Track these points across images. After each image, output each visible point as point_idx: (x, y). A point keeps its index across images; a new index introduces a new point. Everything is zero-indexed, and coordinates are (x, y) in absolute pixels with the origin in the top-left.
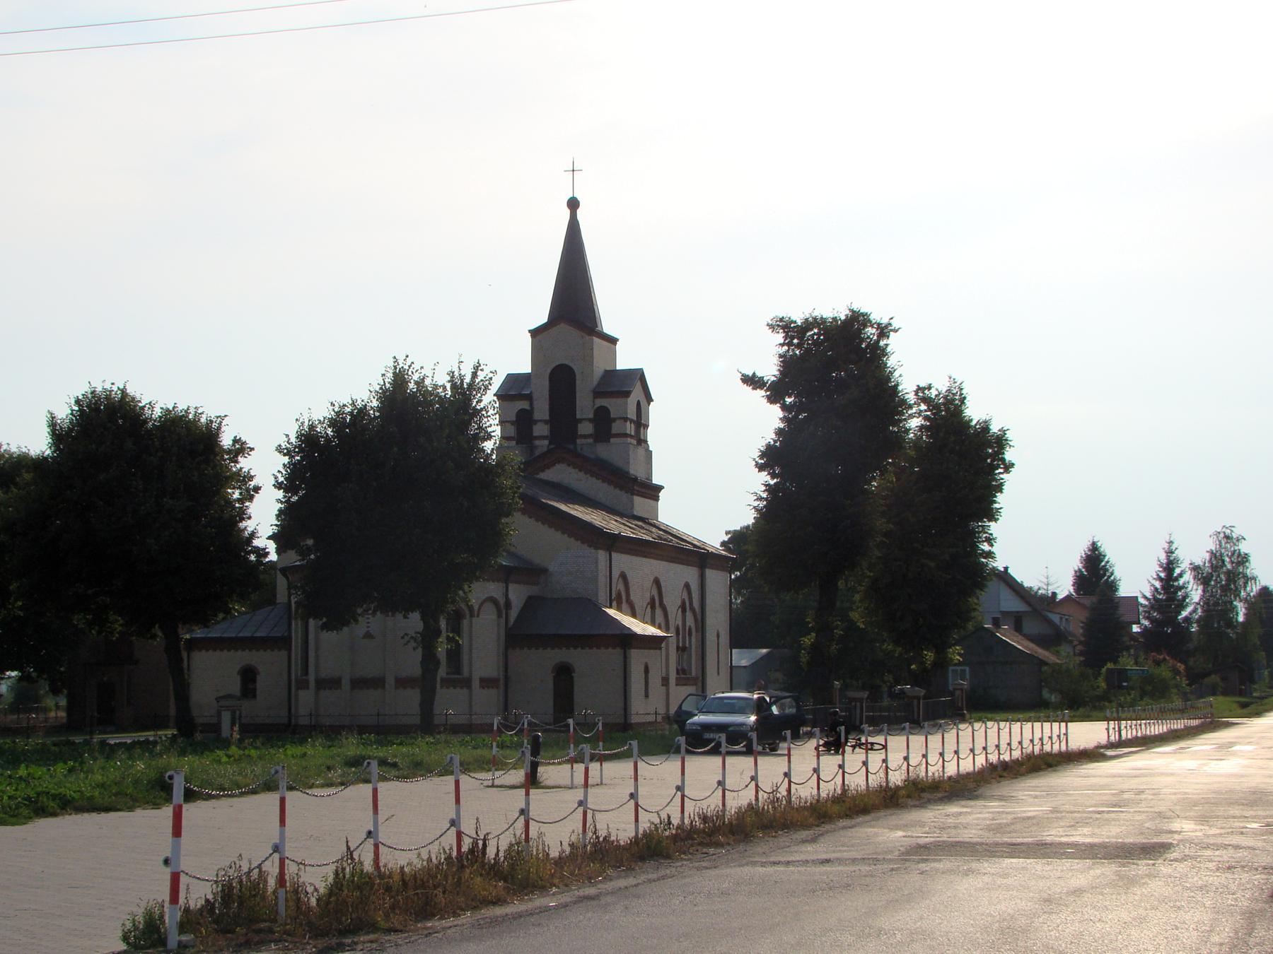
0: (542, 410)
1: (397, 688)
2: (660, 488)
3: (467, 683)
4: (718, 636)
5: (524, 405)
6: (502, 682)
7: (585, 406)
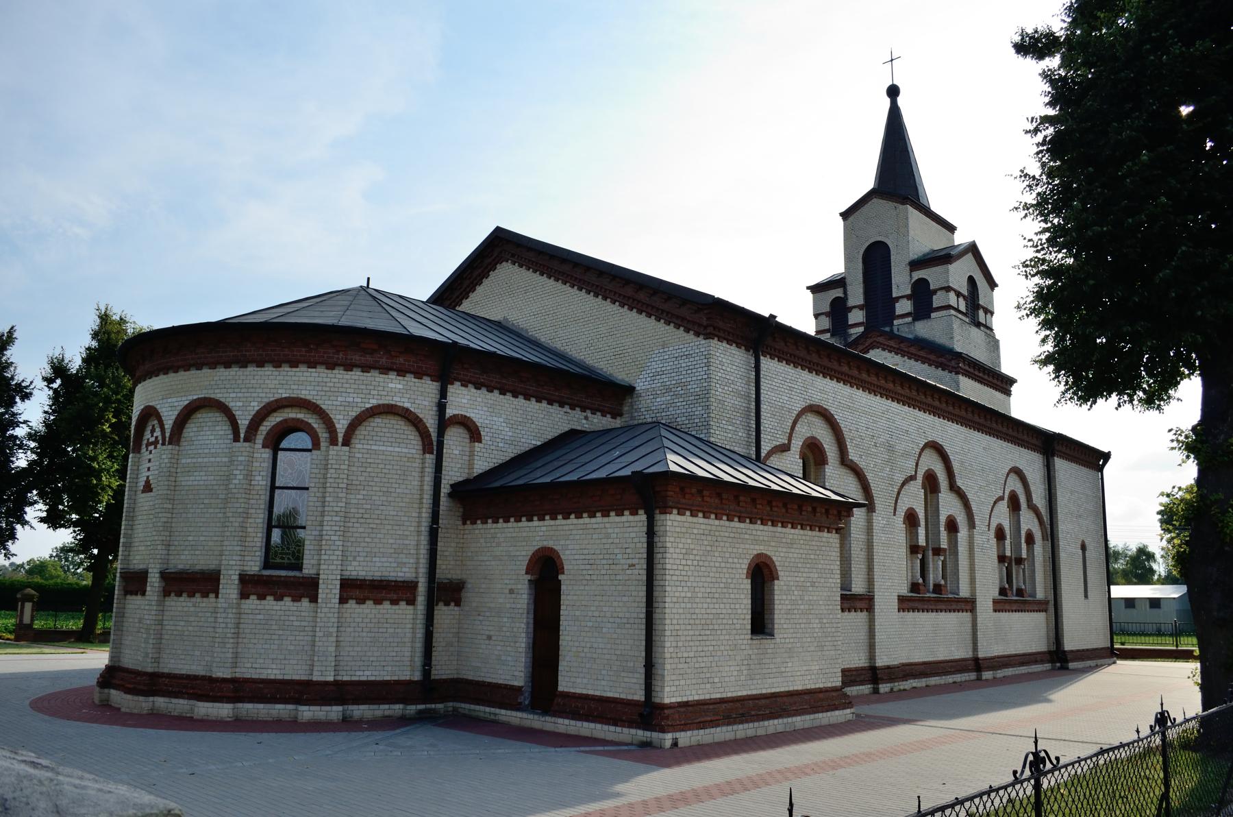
0: (856, 296)
1: (244, 595)
2: (1012, 381)
3: (308, 589)
4: (1083, 548)
5: (838, 293)
6: (422, 588)
7: (901, 282)
